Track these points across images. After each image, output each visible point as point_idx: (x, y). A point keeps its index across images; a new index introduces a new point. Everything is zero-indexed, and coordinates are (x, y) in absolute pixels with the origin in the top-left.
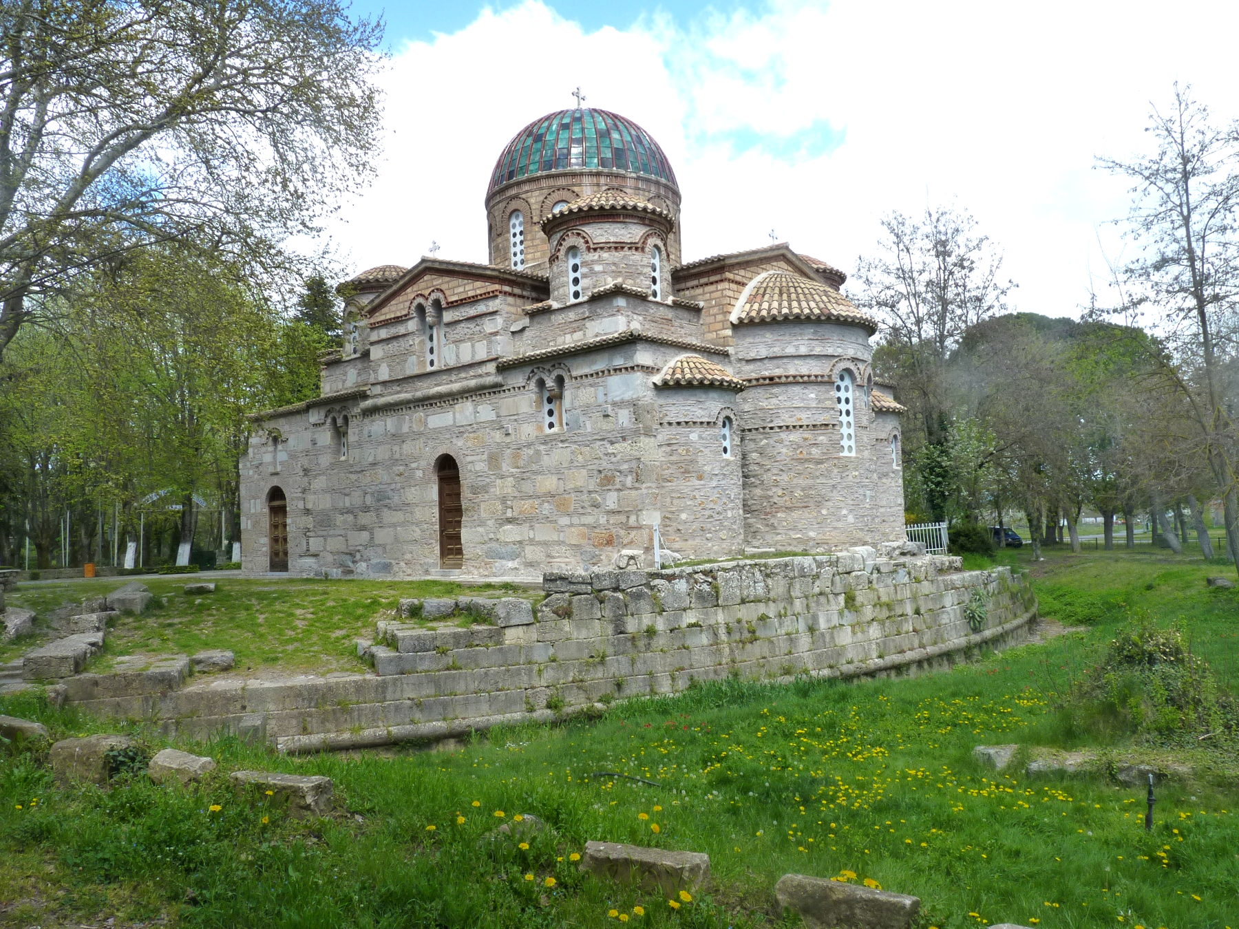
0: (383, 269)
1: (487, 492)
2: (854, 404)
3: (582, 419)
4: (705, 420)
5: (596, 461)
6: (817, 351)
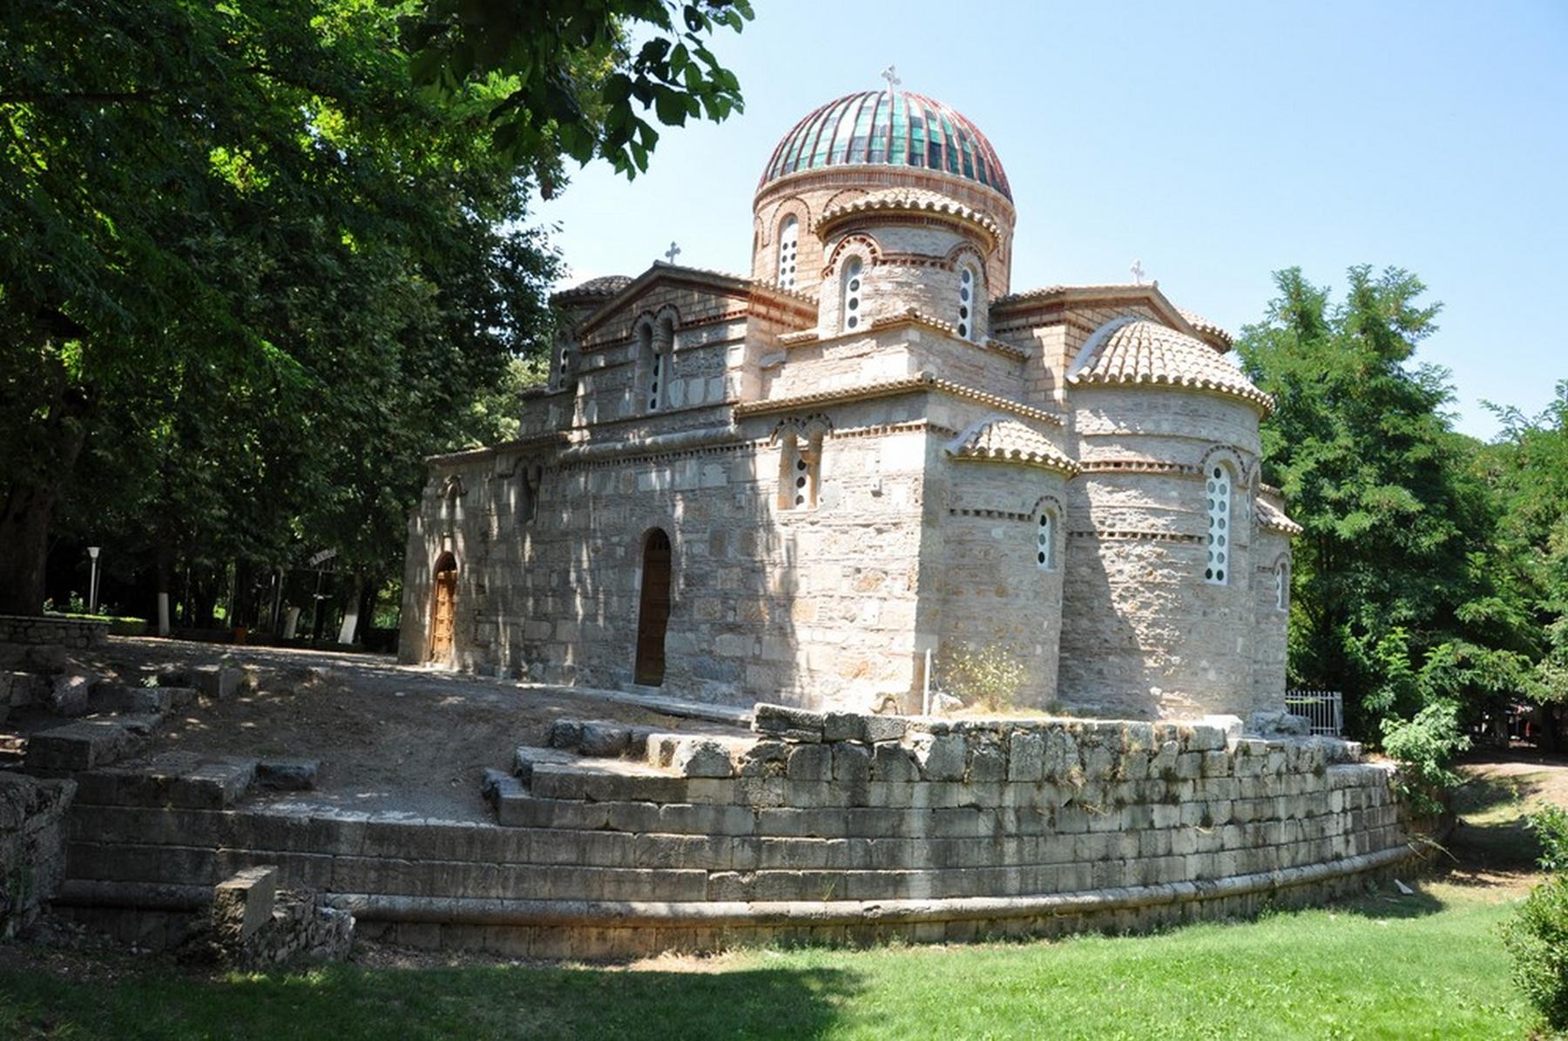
0: (609, 280)
1: (704, 585)
2: (1232, 511)
3: (843, 493)
4: (1017, 511)
5: (852, 555)
6: (1186, 431)
